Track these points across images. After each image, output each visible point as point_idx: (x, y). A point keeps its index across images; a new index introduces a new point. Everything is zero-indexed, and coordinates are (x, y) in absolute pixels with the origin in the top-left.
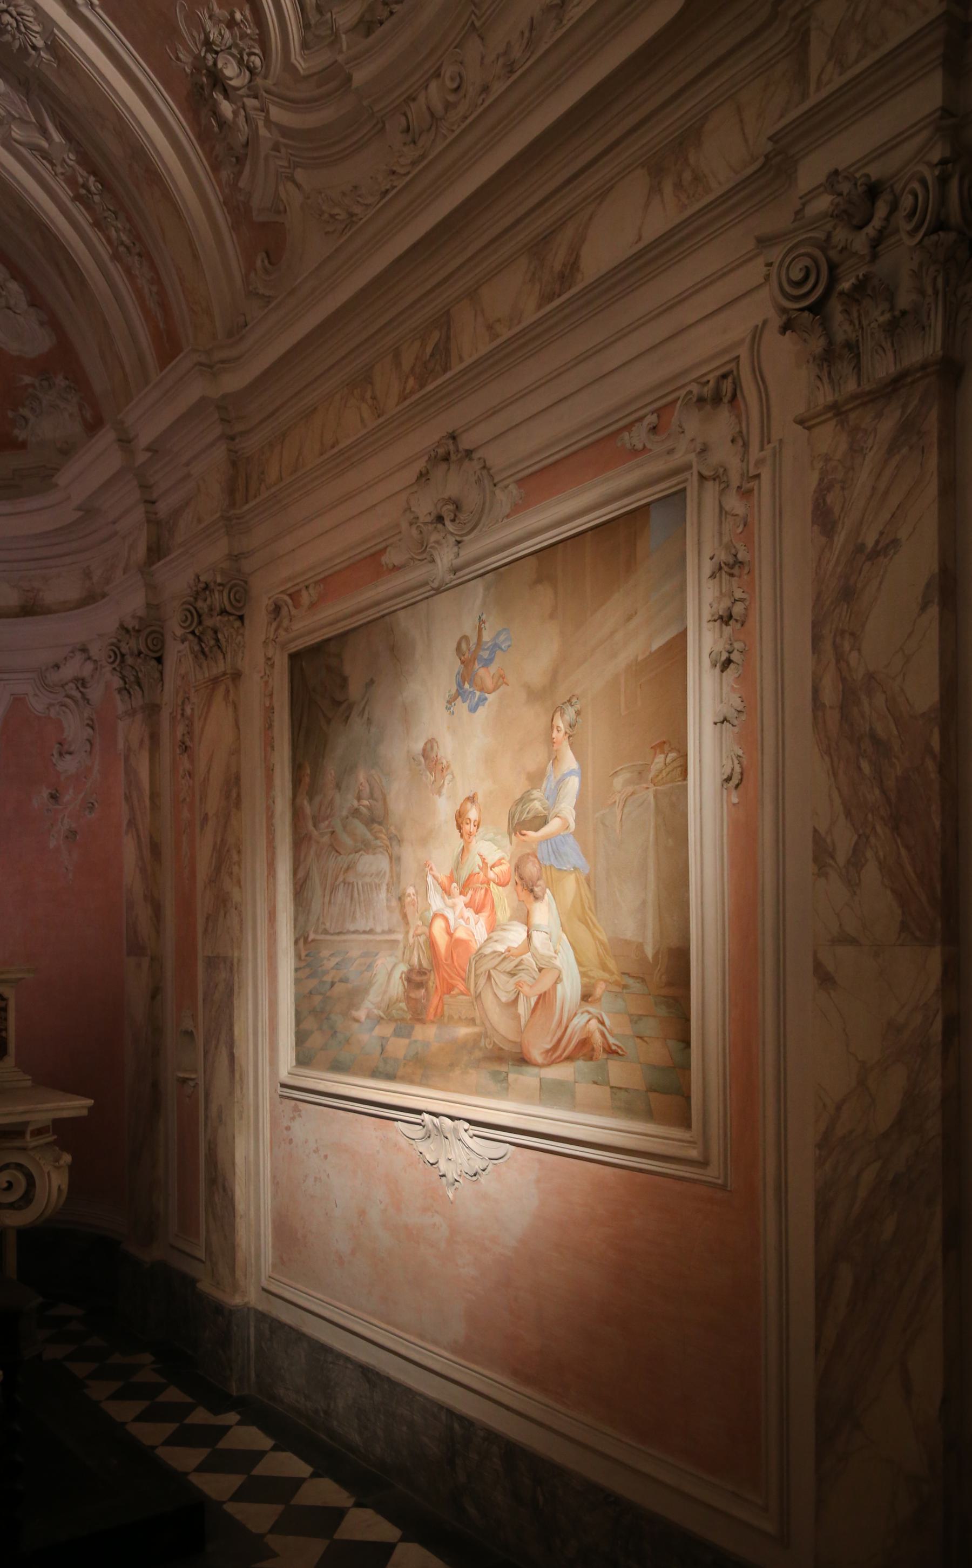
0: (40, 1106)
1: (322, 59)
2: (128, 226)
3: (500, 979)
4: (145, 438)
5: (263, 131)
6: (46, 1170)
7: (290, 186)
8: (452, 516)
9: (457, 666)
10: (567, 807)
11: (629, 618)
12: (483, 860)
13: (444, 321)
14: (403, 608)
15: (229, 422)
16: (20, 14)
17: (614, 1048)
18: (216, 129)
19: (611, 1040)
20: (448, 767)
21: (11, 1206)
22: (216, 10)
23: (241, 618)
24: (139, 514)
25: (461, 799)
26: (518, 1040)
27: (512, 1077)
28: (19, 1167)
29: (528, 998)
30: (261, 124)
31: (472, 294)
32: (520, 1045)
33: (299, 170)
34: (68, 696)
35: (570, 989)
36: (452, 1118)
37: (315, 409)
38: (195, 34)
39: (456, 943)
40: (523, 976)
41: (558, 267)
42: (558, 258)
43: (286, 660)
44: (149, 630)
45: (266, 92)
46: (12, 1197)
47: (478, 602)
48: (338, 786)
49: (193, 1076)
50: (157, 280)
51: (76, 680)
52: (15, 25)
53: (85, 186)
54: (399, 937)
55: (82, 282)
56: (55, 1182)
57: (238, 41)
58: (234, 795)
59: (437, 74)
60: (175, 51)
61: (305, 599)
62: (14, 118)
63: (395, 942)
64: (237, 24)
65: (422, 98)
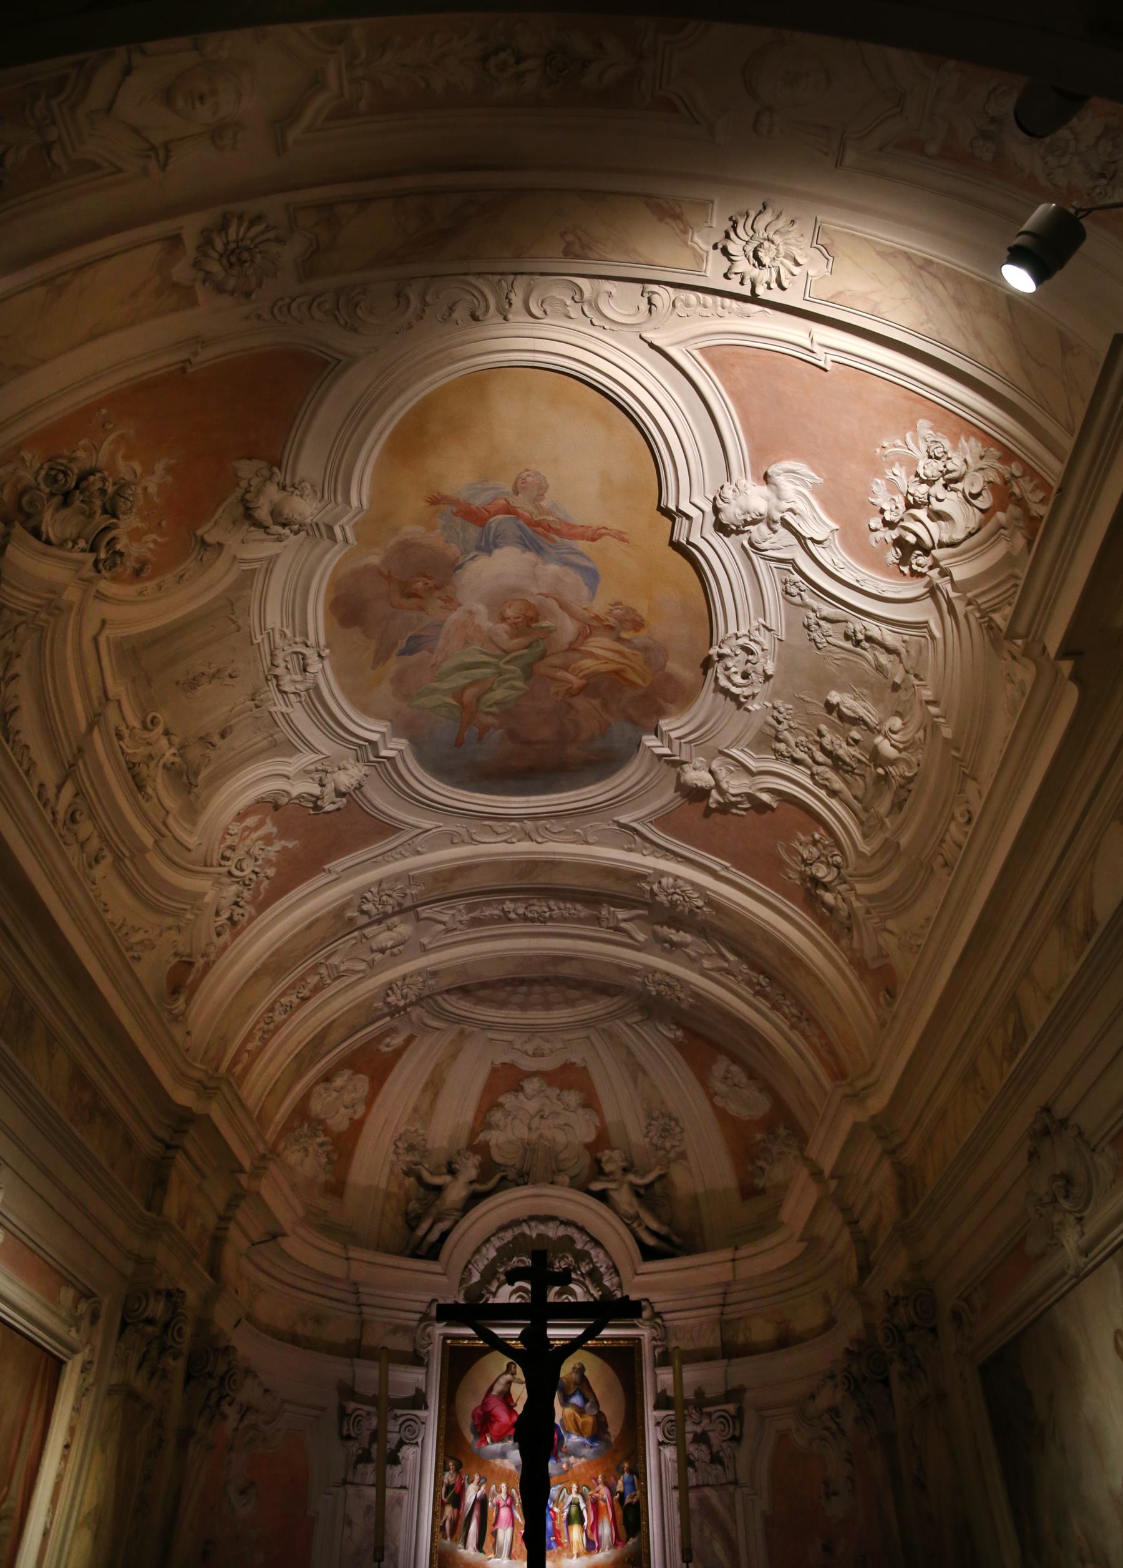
1: (877, 842)
4: (827, 1169)
5: (856, 904)
7: (886, 935)
16: (683, 891)
18: (827, 914)
22: (803, 838)
30: (853, 899)
33: (889, 921)
38: (795, 858)
45: (851, 876)
50: (823, 1035)
52: (681, 899)
53: (759, 984)
55: (773, 1051)
59: (953, 818)
60: (786, 874)
64: (819, 841)
65: (948, 838)
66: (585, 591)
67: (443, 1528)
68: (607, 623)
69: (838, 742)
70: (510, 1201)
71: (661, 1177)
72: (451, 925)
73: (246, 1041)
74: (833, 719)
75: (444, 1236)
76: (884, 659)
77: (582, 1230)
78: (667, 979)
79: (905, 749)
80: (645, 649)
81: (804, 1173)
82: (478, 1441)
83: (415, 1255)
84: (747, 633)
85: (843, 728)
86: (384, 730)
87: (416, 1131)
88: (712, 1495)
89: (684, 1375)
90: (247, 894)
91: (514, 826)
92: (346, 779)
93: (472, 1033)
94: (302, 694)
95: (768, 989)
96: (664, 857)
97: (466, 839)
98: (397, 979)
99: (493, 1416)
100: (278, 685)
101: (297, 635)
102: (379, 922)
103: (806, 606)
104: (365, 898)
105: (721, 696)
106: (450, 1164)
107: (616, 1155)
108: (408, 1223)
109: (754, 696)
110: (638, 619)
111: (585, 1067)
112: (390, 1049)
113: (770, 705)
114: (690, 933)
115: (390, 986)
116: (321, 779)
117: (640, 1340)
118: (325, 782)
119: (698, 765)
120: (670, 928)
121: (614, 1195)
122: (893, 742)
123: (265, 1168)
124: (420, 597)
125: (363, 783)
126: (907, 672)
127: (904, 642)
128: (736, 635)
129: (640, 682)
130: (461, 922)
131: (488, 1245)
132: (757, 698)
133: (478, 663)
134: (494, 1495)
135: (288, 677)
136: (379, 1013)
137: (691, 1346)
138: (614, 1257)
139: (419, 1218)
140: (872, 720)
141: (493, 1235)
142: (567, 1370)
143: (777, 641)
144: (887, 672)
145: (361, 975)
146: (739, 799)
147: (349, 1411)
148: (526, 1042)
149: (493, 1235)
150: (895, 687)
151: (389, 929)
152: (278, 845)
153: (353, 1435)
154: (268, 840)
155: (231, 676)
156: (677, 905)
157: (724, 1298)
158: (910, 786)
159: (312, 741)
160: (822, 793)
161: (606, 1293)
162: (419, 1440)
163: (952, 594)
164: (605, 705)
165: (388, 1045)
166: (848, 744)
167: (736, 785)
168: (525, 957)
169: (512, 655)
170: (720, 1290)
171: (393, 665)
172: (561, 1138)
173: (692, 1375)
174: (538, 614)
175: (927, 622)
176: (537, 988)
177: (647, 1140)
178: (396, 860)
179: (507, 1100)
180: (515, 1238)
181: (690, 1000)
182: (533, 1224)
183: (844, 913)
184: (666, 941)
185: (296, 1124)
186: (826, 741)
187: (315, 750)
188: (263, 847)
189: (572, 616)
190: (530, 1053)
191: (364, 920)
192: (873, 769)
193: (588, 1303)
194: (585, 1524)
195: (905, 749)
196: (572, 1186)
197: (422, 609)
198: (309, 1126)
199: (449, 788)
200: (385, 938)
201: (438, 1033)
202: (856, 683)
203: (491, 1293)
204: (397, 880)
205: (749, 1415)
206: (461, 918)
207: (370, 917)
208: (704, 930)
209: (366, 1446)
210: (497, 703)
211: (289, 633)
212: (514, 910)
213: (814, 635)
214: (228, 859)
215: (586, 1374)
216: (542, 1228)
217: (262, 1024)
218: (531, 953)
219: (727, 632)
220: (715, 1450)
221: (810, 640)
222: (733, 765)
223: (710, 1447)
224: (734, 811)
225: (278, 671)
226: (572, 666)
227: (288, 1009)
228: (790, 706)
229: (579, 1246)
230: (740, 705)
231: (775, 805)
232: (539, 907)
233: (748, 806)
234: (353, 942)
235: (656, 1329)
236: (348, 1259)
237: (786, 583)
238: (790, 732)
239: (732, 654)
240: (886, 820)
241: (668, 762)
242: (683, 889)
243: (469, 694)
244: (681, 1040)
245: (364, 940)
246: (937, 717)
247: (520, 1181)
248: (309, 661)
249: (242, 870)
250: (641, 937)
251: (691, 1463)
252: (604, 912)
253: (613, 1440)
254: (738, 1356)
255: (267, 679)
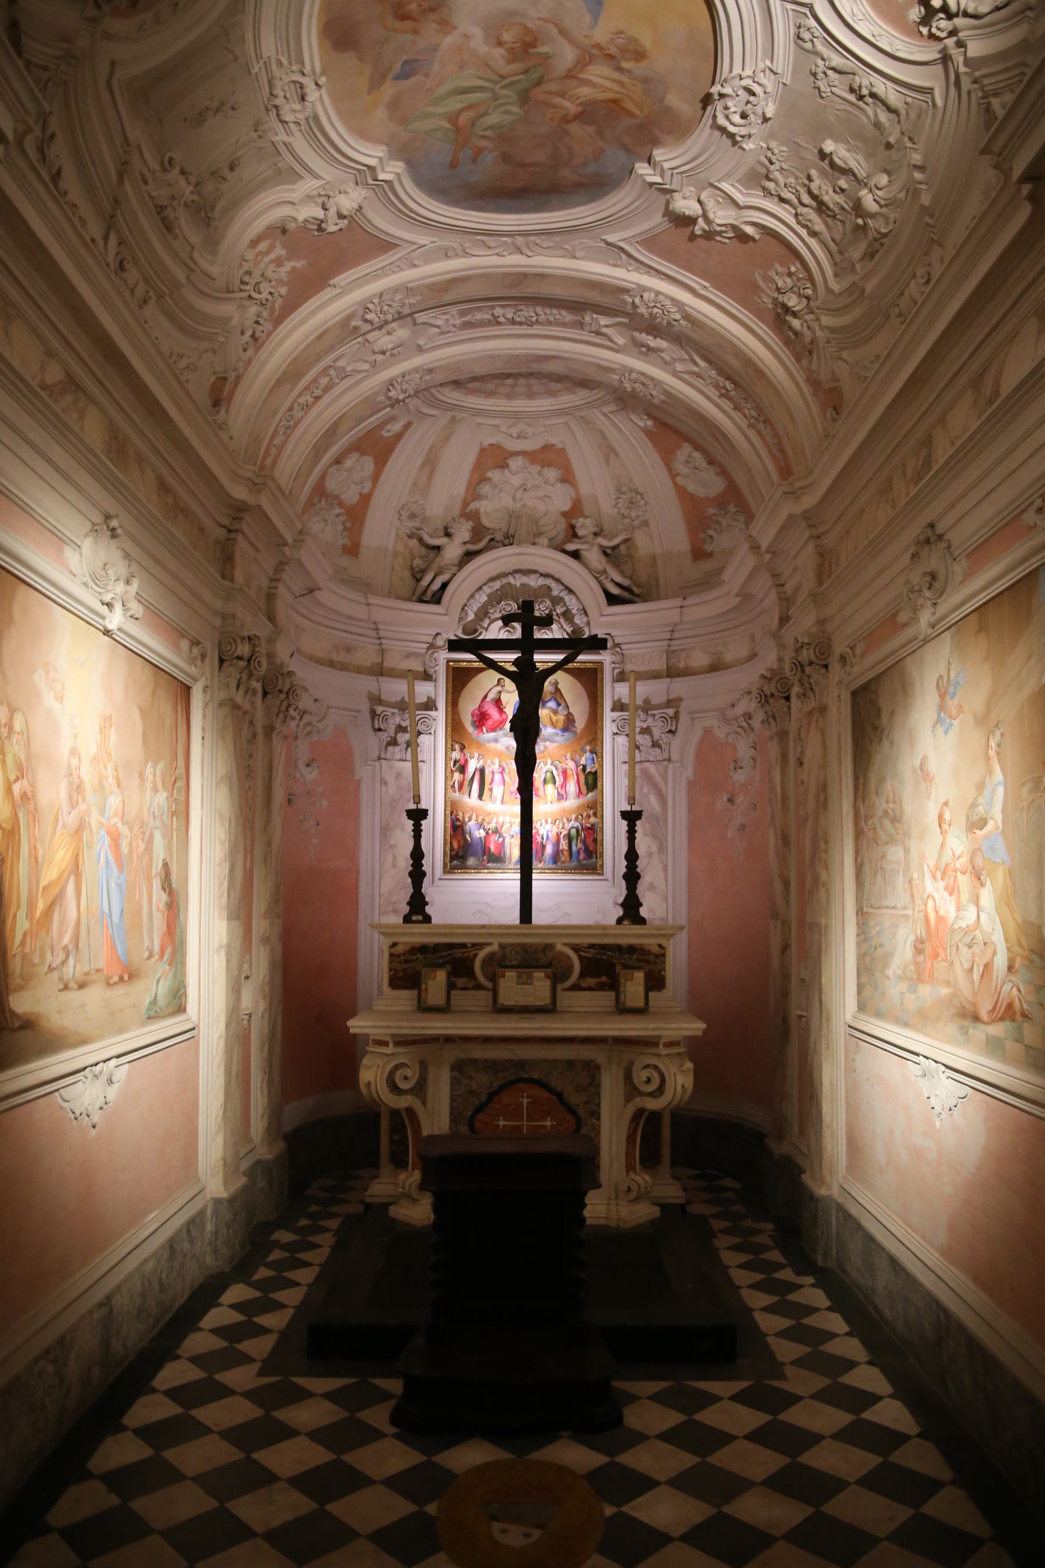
0: (667, 1026)
2: (754, 405)
3: (963, 949)
6: (672, 1072)
8: (927, 585)
9: (937, 699)
10: (997, 812)
11: (1029, 658)
12: (953, 852)
13: (928, 441)
14: (909, 654)
15: (815, 526)
17: (1026, 1012)
18: (793, 337)
19: (1025, 1006)
20: (934, 778)
21: (651, 1095)
22: (779, 269)
23: (826, 666)
24: (773, 595)
25: (941, 802)
26: (973, 1001)
27: (971, 1031)
28: (656, 1068)
29: (978, 966)
30: (817, 329)
31: (942, 420)
32: (974, 1004)
34: (740, 727)
35: (1001, 962)
36: (936, 1062)
37: (863, 512)
38: (770, 285)
39: (940, 919)
40: (977, 949)
41: (988, 393)
42: (987, 390)
43: (849, 696)
44: (779, 677)
45: (818, 308)
46: (651, 1088)
47: (948, 648)
48: (877, 793)
49: (805, 1014)
50: (776, 436)
51: (744, 715)
53: (725, 388)
54: (909, 912)
55: (732, 446)
56: (680, 1082)
57: (796, 283)
58: (822, 799)
59: (914, 276)
60: (760, 298)
61: (858, 650)
62: (676, 360)
63: (907, 916)
64: (794, 274)
66: (587, 19)
67: (453, 786)
68: (607, 52)
69: (826, 188)
70: (500, 557)
71: (626, 541)
72: (444, 329)
73: (273, 436)
74: (825, 166)
75: (444, 586)
76: (883, 117)
77: (558, 580)
78: (642, 378)
79: (886, 205)
80: (646, 80)
81: (745, 547)
82: (477, 731)
83: (421, 601)
84: (751, 74)
85: (833, 175)
86: (381, 155)
87: (416, 502)
88: (652, 768)
89: (637, 688)
90: (265, 314)
91: (506, 241)
92: (347, 202)
93: (462, 419)
94: (302, 123)
95: (733, 393)
96: (647, 273)
97: (460, 252)
98: (397, 377)
99: (488, 715)
100: (278, 115)
101: (293, 62)
102: (380, 328)
103: (816, 53)
104: (368, 308)
105: (717, 133)
106: (446, 528)
107: (588, 522)
108: (413, 575)
109: (750, 136)
110: (640, 49)
111: (563, 448)
112: (391, 434)
113: (764, 146)
114: (666, 340)
115: (391, 383)
116: (323, 204)
117: (602, 663)
118: (327, 207)
119: (688, 194)
120: (648, 335)
121: (585, 554)
122: (876, 197)
123: (302, 541)
124: (414, 20)
125: (363, 206)
126: (903, 134)
127: (906, 103)
128: (740, 76)
129: (637, 112)
130: (454, 325)
131: (480, 592)
132: (752, 138)
133: (474, 87)
134: (489, 766)
135: (287, 107)
136: (382, 406)
137: (642, 668)
138: (583, 602)
139: (423, 572)
140: (861, 173)
141: (485, 584)
142: (548, 686)
143: (781, 85)
144: (884, 130)
145: (365, 374)
146: (724, 229)
147: (378, 712)
148: (511, 426)
149: (485, 584)
150: (889, 146)
151: (389, 333)
152: (288, 266)
153: (383, 728)
154: (279, 262)
155: (233, 109)
156: (656, 318)
157: (672, 635)
158: (884, 240)
159: (314, 169)
160: (803, 232)
161: (577, 630)
162: (432, 731)
163: (962, 69)
164: (600, 133)
165: (389, 431)
166: (834, 191)
167: (722, 216)
168: (512, 356)
169: (509, 80)
170: (670, 629)
171: (389, 90)
172: (541, 507)
173: (644, 689)
174: (535, 39)
175: (932, 89)
176: (522, 381)
177: (616, 510)
178: (394, 272)
179: (495, 475)
180: (502, 587)
181: (662, 397)
182: (517, 576)
183: (808, 340)
184: (643, 346)
185: (316, 500)
186: (814, 186)
187: (317, 177)
188: (275, 269)
189: (572, 42)
190: (515, 435)
191: (368, 327)
192: (854, 218)
193: (564, 639)
194: (557, 784)
195: (886, 205)
196: (550, 546)
197: (416, 32)
198: (326, 501)
199: (444, 207)
200: (384, 341)
201: (432, 419)
202: (854, 135)
203: (483, 628)
204: (396, 292)
205: (684, 717)
206: (454, 322)
207: (372, 324)
208: (678, 339)
209: (393, 735)
210: (491, 127)
211: (285, 61)
212: (504, 316)
213: (820, 83)
214: (247, 284)
215: (559, 686)
216: (525, 579)
217: (284, 422)
218: (517, 352)
219: (731, 71)
220: (655, 739)
221: (815, 88)
222: (723, 198)
223: (652, 737)
224: (718, 238)
225: (278, 101)
226: (570, 93)
227: (305, 407)
228: (785, 149)
229: (555, 593)
230: (735, 143)
231: (757, 237)
232: (527, 312)
233: (732, 235)
234: (358, 346)
235: (615, 655)
236: (368, 605)
237: (799, 27)
238: (781, 173)
239: (734, 95)
240: (858, 266)
241: (659, 190)
242: (663, 304)
243: (464, 119)
244: (651, 428)
245: (367, 344)
246: (920, 183)
247: (507, 542)
248: (307, 90)
249: (260, 293)
250: (621, 341)
251: (637, 747)
252: (588, 319)
253: (579, 731)
254: (678, 676)
255: (267, 109)
